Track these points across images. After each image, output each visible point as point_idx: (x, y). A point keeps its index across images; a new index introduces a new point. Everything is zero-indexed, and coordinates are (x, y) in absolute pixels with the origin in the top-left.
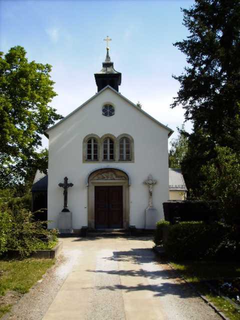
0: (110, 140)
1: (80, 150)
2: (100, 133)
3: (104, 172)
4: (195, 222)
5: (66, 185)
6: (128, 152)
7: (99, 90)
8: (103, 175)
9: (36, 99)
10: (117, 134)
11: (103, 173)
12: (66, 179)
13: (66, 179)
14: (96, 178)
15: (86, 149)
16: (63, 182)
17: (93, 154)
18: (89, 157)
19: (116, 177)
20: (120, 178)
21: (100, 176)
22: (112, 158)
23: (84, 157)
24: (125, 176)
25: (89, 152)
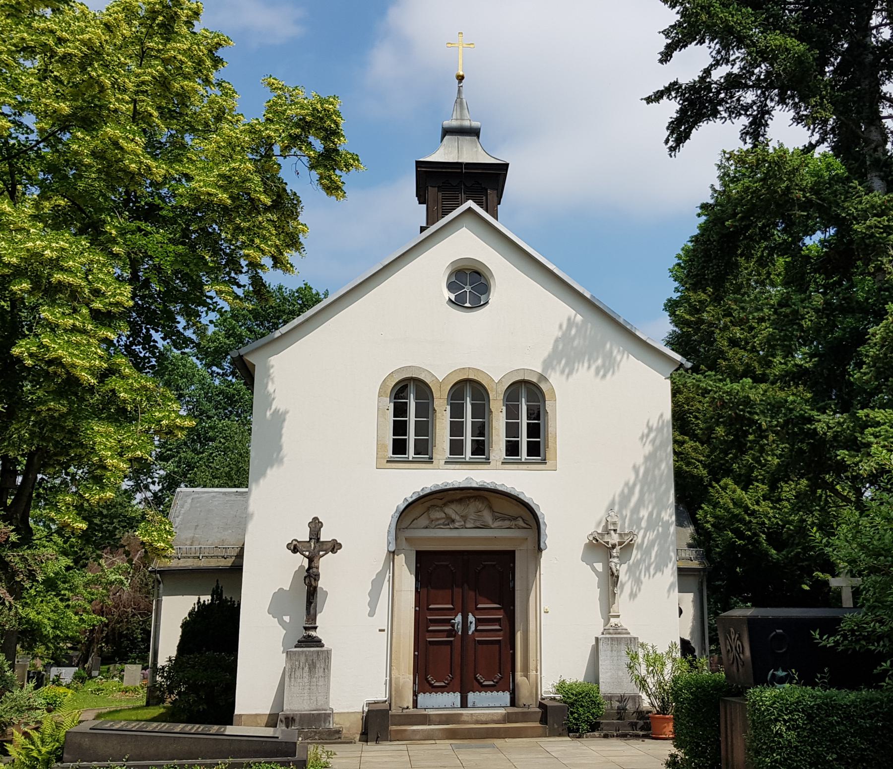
0: (469, 390)
1: (373, 422)
2: (440, 371)
3: (452, 502)
4: (852, 696)
5: (315, 546)
6: (534, 430)
7: (431, 219)
8: (447, 510)
9: (233, 275)
10: (497, 373)
11: (445, 505)
12: (316, 526)
13: (316, 526)
14: (423, 521)
15: (390, 418)
16: (304, 535)
17: (411, 437)
18: (399, 447)
19: (495, 519)
20: (507, 523)
21: (437, 514)
22: (480, 448)
23: (380, 446)
24: (524, 515)
25: (400, 428)
